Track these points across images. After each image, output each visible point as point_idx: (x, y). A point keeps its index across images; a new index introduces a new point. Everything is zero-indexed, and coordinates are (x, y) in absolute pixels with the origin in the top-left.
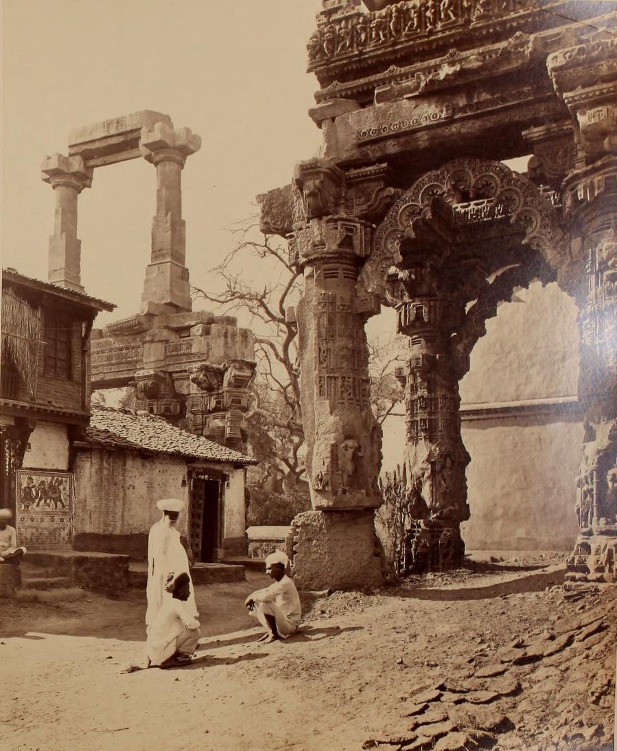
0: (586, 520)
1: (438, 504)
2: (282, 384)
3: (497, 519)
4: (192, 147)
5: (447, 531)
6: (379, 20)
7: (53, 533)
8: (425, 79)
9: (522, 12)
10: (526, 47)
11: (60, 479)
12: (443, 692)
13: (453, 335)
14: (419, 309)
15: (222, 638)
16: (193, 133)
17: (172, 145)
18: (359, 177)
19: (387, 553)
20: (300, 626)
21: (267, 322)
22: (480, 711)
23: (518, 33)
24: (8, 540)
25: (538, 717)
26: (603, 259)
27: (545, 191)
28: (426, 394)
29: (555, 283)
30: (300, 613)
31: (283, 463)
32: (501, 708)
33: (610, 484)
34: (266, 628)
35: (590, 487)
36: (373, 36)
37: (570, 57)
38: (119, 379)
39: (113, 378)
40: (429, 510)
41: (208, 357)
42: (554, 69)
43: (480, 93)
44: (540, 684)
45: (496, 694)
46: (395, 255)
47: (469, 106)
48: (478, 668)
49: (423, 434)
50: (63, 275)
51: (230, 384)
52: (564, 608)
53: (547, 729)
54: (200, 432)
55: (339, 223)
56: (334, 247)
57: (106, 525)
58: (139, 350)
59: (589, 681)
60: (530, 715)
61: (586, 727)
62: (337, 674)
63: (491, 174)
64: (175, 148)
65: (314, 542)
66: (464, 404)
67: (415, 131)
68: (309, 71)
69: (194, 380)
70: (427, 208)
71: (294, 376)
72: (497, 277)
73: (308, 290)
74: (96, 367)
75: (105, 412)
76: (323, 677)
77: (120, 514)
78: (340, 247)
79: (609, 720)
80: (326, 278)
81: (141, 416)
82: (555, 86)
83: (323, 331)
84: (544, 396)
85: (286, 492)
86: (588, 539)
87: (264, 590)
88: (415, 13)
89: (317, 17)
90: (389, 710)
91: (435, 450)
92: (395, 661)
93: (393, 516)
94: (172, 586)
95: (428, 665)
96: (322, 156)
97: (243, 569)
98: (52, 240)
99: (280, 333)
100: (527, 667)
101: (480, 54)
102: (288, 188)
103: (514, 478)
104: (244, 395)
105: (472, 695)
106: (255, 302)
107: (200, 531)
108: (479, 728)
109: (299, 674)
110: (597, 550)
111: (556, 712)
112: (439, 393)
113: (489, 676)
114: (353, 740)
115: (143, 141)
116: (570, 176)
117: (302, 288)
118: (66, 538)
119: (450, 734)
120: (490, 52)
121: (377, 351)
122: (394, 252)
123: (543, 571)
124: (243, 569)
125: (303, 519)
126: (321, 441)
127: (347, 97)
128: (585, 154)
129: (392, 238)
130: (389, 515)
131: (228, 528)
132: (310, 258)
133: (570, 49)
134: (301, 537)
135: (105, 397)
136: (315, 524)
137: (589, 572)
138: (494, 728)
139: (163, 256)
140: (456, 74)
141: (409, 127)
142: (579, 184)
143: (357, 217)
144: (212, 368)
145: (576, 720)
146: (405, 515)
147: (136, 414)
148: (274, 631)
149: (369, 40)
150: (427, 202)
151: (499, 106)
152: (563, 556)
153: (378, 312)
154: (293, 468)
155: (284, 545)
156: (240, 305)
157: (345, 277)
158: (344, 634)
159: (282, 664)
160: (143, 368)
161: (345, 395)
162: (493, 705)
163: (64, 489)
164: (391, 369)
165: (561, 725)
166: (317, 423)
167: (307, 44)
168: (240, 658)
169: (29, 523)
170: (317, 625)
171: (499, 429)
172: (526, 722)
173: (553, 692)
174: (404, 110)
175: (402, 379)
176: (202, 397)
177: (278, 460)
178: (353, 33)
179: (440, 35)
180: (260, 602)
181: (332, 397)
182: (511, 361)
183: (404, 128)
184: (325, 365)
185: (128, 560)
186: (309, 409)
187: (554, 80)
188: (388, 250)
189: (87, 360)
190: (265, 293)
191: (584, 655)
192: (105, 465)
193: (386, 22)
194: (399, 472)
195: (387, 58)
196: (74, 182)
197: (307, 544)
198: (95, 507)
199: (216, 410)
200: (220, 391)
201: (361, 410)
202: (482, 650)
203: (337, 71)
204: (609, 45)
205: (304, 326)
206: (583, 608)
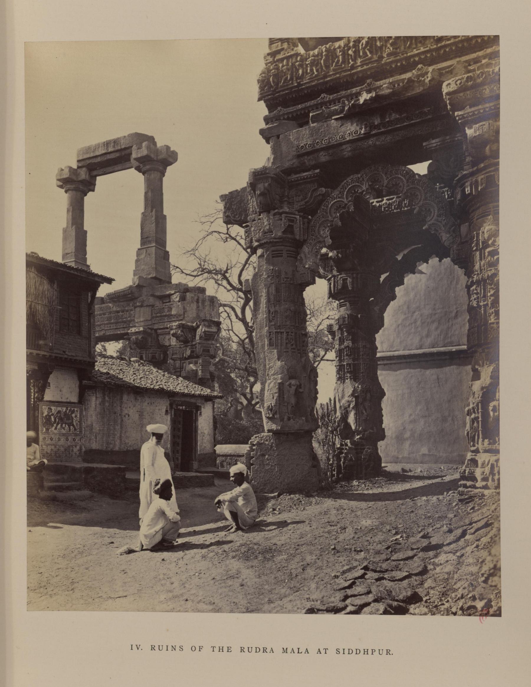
0: (473, 440)
1: (361, 428)
2: (241, 337)
3: (407, 439)
4: (171, 160)
5: (368, 448)
6: (313, 58)
7: (68, 449)
8: (349, 104)
9: (422, 49)
10: (426, 77)
11: (72, 409)
12: (367, 572)
13: (371, 299)
14: (345, 280)
15: (197, 528)
16: (172, 149)
17: (155, 159)
18: (298, 180)
19: (322, 466)
20: (257, 520)
21: (228, 291)
22: (395, 586)
23: (420, 66)
24: (33, 454)
25: (440, 592)
26: (485, 239)
27: (441, 188)
28: (351, 344)
29: (449, 259)
30: (257, 510)
31: (242, 397)
32: (412, 585)
33: (491, 414)
34: (230, 521)
35: (477, 415)
36: (308, 71)
37: (460, 84)
38: (117, 334)
39: (112, 333)
40: (354, 432)
41: (184, 318)
42: (448, 94)
43: (391, 114)
44: (441, 567)
45: (407, 573)
46: (326, 240)
47: (383, 124)
48: (393, 553)
49: (348, 375)
50: (73, 257)
51: (201, 337)
52: (459, 508)
53: (448, 601)
54: (178, 374)
55: (283, 215)
56: (280, 234)
57: (108, 443)
58: (132, 312)
59: (479, 565)
60: (434, 590)
61: (478, 600)
62: (285, 557)
63: (400, 176)
64: (158, 161)
65: (267, 456)
66: (380, 352)
67: (341, 144)
68: (259, 100)
69: (173, 335)
70: (351, 203)
71: (249, 330)
72: (404, 254)
73: (260, 266)
74: (99, 325)
75: (107, 359)
76: (275, 559)
77: (118, 435)
78: (283, 234)
79: (496, 596)
80: (273, 257)
81: (134, 361)
82: (449, 107)
83: (272, 297)
84: (441, 346)
85: (245, 419)
86: (475, 455)
87: (229, 493)
88: (340, 51)
89: (265, 58)
90: (325, 585)
91: (358, 387)
92: (330, 548)
93: (326, 437)
94: (158, 489)
95: (355, 551)
96: (270, 165)
97: (213, 477)
98: (65, 231)
99: (239, 299)
100: (431, 553)
101: (390, 83)
102: (244, 189)
103: (419, 408)
104: (212, 346)
105: (389, 574)
106: (220, 276)
107: (179, 448)
108: (394, 600)
109: (256, 556)
110: (483, 464)
111: (454, 589)
112: (361, 344)
113: (402, 560)
114: (298, 608)
115: (134, 156)
116: (459, 176)
117: (255, 265)
118: (78, 453)
119: (372, 605)
120: (398, 82)
121: (313, 312)
122: (326, 237)
123: (442, 479)
124: (213, 477)
125: (257, 440)
126: (271, 380)
127: (288, 119)
128: (471, 159)
129: (324, 226)
130: (324, 437)
131: (201, 446)
132: (261, 242)
133: (460, 77)
134: (257, 453)
135: (106, 348)
136: (267, 443)
137: (477, 481)
138: (406, 600)
139: (150, 242)
140: (372, 99)
141: (336, 141)
142: (467, 182)
143: (296, 210)
144: (188, 326)
145: (470, 595)
146: (335, 436)
147: (130, 361)
148: (237, 524)
149: (305, 74)
150: (350, 199)
151: (405, 124)
152: (457, 468)
153: (314, 282)
154: (249, 401)
155: (243, 459)
156: (207, 279)
157: (288, 257)
158: (290, 527)
159: (243, 549)
160: (135, 326)
161: (289, 345)
162: (406, 581)
163: (76, 416)
164: (324, 326)
165: (459, 599)
166: (267, 367)
167: (258, 79)
168: (211, 544)
169: (49, 442)
170: (270, 519)
171: (407, 371)
172: (431, 595)
173: (452, 573)
174: (332, 128)
175: (332, 332)
176: (180, 347)
177: (238, 395)
178: (293, 69)
179: (359, 69)
180: (226, 501)
181: (279, 347)
182: (416, 319)
183: (333, 142)
184: (273, 323)
185: (124, 470)
186: (262, 356)
187: (448, 102)
188: (321, 236)
189: (92, 320)
190: (227, 269)
191: (475, 545)
192: (107, 398)
193: (318, 60)
194: (331, 404)
195: (320, 88)
196: (81, 187)
197: (261, 459)
198: (100, 430)
199: (190, 357)
200: (194, 343)
201: (301, 357)
202: (396, 540)
203: (281, 99)
204: (491, 73)
205: (258, 293)
206: (473, 508)
